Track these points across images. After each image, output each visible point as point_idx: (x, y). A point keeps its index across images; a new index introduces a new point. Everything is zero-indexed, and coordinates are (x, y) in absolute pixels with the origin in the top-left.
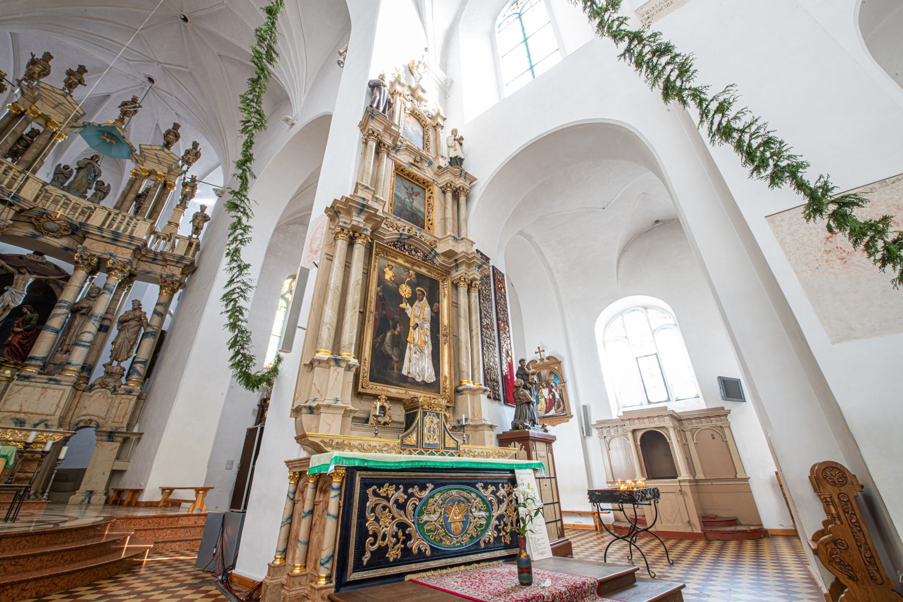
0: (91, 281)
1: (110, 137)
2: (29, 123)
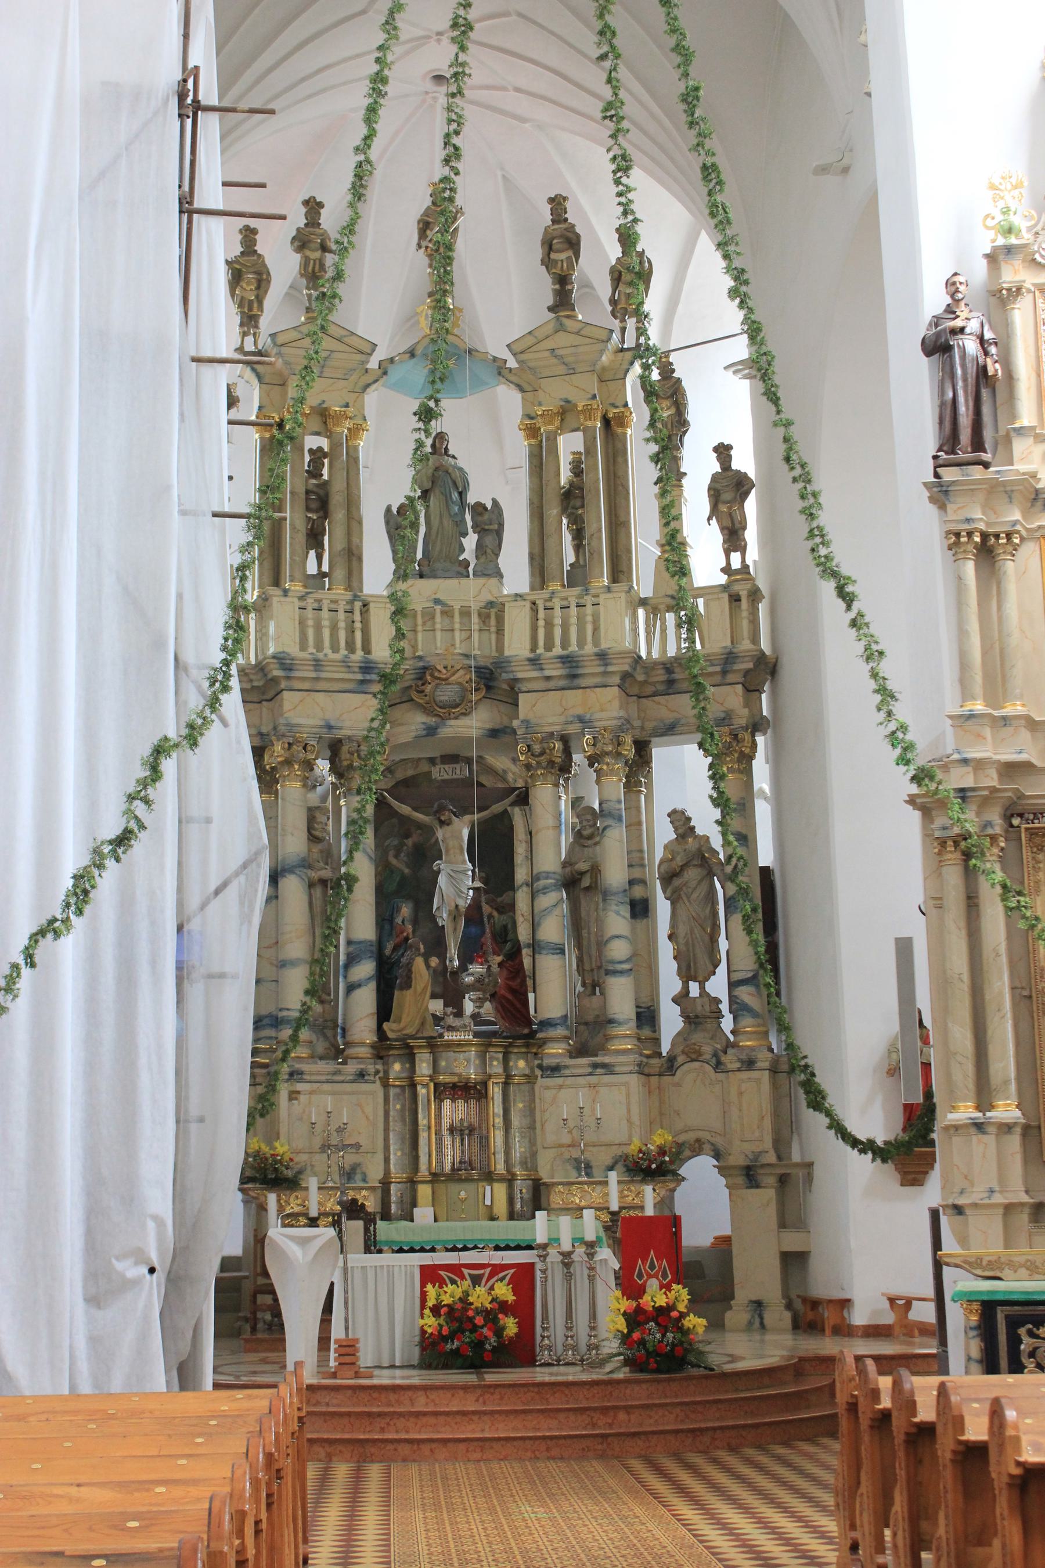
1: (443, 356)
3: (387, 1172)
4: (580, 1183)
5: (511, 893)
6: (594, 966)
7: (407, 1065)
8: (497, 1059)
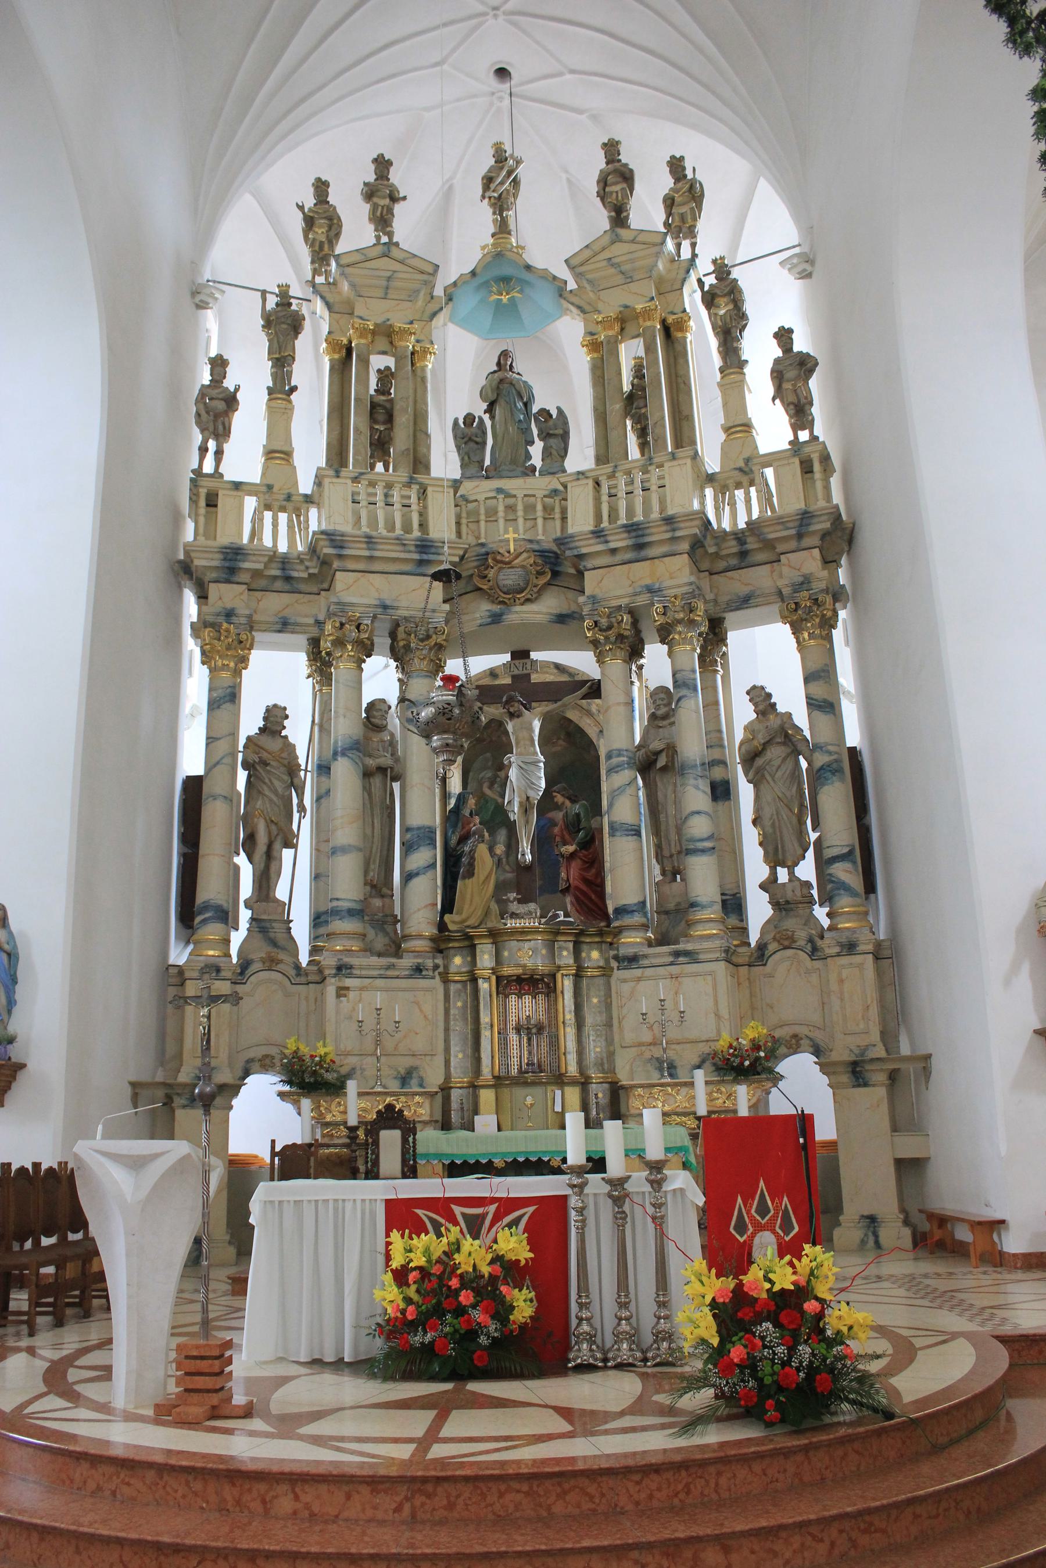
0: (640, 676)
1: (504, 277)
2: (365, 362)
3: (448, 1077)
4: (662, 1085)
5: (599, 818)
7: (469, 959)
8: (567, 949)
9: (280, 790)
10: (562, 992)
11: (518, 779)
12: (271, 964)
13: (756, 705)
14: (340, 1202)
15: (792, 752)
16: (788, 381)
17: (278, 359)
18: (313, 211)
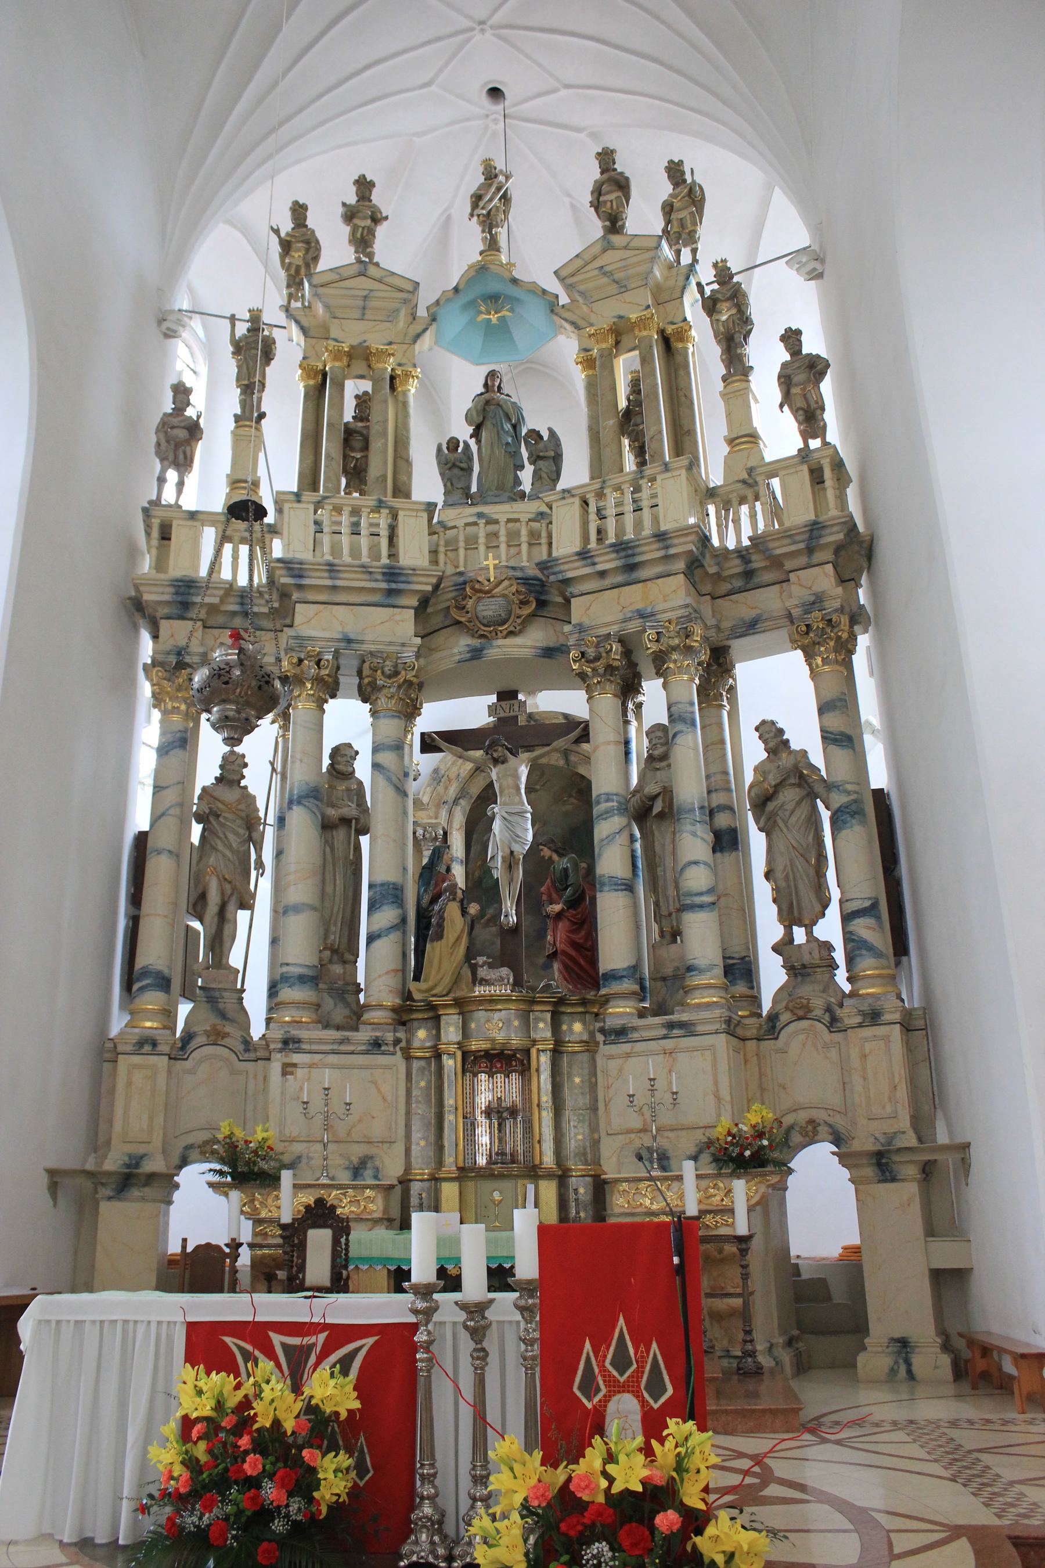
1: (491, 295)
2: (340, 387)
6: (672, 909)
7: (434, 1032)
9: (234, 845)
10: (538, 1070)
11: (501, 831)
12: (216, 1037)
13: (765, 742)
14: (131, 1325)
15: (808, 794)
16: (796, 385)
17: (246, 385)
18: (292, 236)
